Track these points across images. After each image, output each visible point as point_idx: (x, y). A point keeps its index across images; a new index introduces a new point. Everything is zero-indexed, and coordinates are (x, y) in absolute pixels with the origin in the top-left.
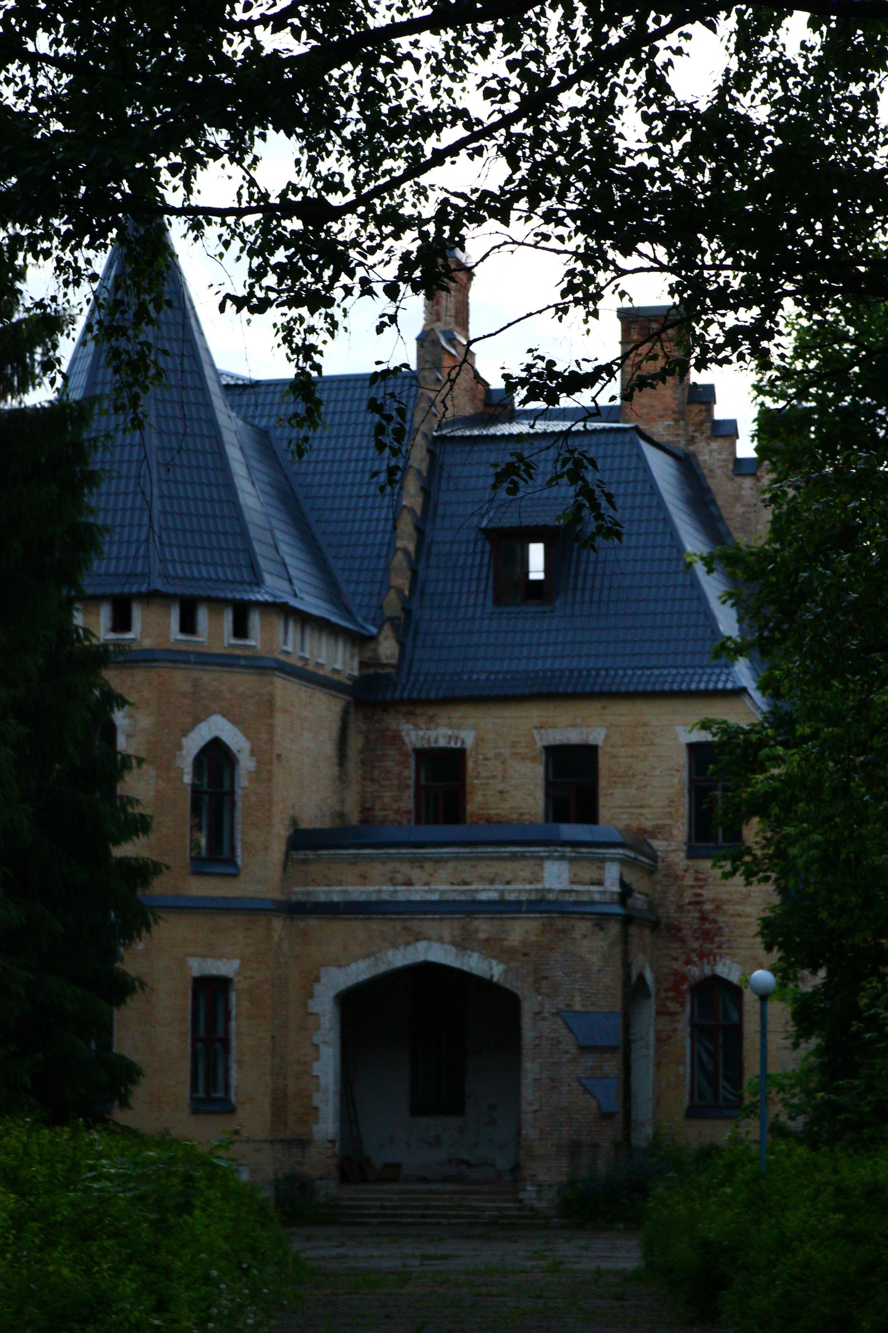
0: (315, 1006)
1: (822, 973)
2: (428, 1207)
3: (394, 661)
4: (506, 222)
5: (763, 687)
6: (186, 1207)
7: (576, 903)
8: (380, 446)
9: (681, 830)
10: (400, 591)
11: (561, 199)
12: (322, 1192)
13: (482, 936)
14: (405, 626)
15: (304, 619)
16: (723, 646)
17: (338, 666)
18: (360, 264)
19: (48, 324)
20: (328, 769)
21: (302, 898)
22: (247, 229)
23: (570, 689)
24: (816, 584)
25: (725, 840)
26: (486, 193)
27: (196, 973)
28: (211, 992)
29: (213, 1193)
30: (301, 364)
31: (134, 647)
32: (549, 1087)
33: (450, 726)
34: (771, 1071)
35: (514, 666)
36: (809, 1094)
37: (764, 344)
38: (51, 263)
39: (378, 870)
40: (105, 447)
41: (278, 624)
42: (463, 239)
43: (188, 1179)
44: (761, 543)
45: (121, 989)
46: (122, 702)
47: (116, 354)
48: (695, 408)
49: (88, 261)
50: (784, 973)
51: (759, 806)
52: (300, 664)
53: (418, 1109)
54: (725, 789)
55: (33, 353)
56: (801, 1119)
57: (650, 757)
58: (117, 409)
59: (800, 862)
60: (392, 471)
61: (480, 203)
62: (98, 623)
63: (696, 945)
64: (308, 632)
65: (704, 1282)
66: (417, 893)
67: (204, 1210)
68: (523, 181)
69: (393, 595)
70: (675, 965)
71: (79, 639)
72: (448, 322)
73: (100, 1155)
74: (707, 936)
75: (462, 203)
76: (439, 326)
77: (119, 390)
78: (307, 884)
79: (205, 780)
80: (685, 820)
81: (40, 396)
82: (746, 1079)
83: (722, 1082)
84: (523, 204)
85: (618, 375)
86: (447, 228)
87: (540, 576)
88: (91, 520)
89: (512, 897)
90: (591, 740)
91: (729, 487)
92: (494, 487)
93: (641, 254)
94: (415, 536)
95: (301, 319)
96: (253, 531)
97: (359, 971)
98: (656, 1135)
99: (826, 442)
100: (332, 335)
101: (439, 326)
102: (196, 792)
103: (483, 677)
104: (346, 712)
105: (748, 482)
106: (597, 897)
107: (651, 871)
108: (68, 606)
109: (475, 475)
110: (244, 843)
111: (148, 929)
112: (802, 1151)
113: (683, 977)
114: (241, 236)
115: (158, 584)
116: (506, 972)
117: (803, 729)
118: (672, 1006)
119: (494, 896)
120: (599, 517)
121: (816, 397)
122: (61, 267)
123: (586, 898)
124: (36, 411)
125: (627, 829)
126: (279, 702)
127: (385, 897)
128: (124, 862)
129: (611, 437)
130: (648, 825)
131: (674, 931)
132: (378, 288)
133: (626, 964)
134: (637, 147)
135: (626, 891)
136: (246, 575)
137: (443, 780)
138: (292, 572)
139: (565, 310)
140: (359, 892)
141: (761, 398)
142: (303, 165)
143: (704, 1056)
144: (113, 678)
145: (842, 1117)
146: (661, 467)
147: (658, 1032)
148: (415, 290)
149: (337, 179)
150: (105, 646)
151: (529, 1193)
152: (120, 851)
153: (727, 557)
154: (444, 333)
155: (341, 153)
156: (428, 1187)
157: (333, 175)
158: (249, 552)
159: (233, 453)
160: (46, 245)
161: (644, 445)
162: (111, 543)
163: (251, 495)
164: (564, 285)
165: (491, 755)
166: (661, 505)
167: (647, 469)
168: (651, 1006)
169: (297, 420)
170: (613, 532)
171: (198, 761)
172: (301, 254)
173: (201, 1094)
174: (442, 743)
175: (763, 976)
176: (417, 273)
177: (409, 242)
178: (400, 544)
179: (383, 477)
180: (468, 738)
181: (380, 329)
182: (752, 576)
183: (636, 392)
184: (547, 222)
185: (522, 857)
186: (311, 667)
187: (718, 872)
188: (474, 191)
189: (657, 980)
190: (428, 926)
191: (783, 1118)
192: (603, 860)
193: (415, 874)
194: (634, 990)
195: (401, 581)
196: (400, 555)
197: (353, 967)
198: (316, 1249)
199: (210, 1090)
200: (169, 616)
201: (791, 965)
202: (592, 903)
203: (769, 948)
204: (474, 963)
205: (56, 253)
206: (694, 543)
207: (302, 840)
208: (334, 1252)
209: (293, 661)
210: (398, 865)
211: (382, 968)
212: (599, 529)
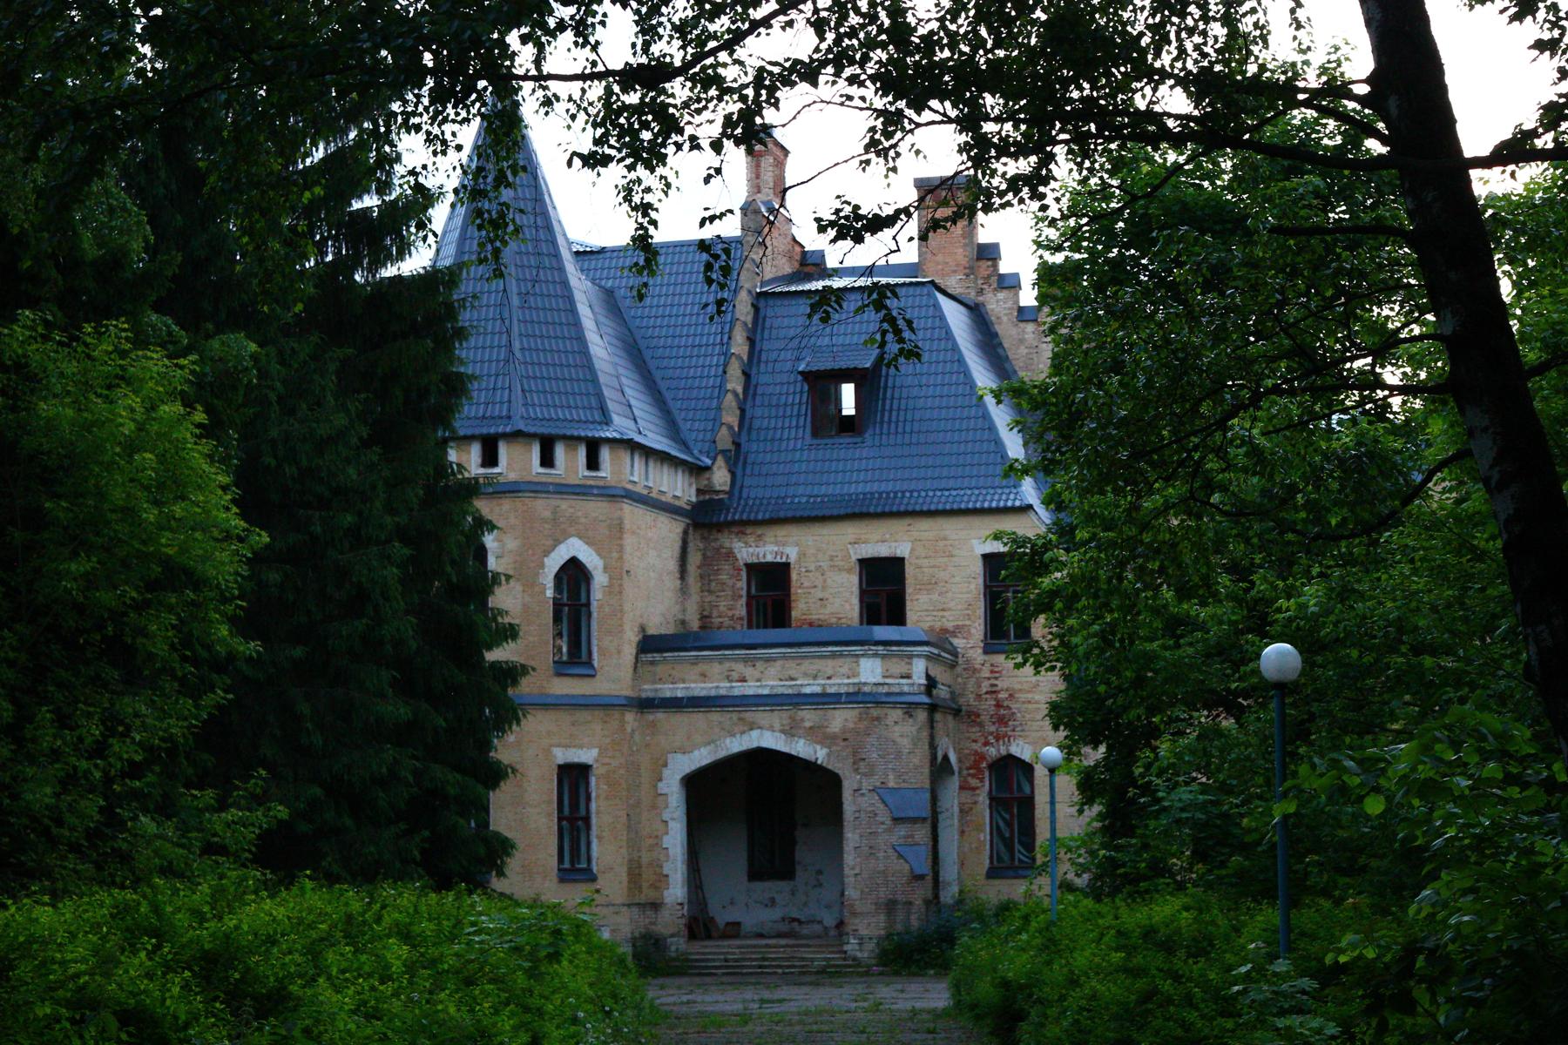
0: (662, 787)
1: (1102, 749)
2: (764, 959)
3: (727, 488)
4: (815, 84)
5: (1046, 502)
6: (555, 957)
7: (888, 694)
8: (709, 281)
9: (978, 629)
10: (730, 428)
11: (862, 67)
12: (673, 948)
13: (808, 724)
14: (736, 458)
15: (648, 453)
16: (1011, 467)
17: (678, 493)
18: (689, 123)
19: (424, 197)
20: (672, 582)
21: (651, 695)
22: (591, 104)
23: (879, 510)
24: (1090, 403)
25: (1016, 637)
26: (797, 62)
27: (561, 761)
28: (573, 778)
29: (577, 948)
30: (640, 220)
31: (501, 480)
32: (869, 856)
33: (776, 543)
34: (1059, 835)
35: (830, 490)
36: (1093, 853)
37: (1041, 189)
38: (422, 136)
39: (716, 669)
40: (473, 307)
41: (625, 456)
42: (777, 100)
43: (557, 933)
44: (1043, 376)
45: (495, 775)
46: (492, 527)
47: (479, 213)
48: (985, 264)
49: (454, 134)
50: (1070, 750)
51: (1044, 606)
52: (645, 492)
53: (755, 875)
54: (1016, 592)
55: (408, 227)
56: (1086, 876)
57: (949, 568)
58: (481, 261)
59: (1081, 650)
60: (720, 303)
61: (792, 70)
62: (469, 461)
63: (993, 729)
64: (651, 464)
65: (1005, 1015)
66: (750, 689)
67: (571, 962)
68: (829, 50)
69: (724, 430)
70: (975, 746)
71: (453, 473)
72: (767, 194)
73: (480, 914)
74: (1002, 721)
75: (776, 70)
76: (760, 197)
77: (481, 245)
78: (654, 682)
79: (565, 595)
80: (982, 621)
81: (418, 260)
82: (1038, 843)
83: (1017, 846)
84: (830, 69)
85: (915, 216)
86: (764, 92)
87: (852, 412)
88: (462, 370)
89: (832, 690)
90: (899, 554)
91: (1014, 331)
92: (810, 316)
93: (931, 109)
94: (742, 379)
95: (639, 181)
96: (602, 379)
97: (702, 757)
98: (961, 892)
99: (1099, 288)
100: (666, 194)
101: (760, 197)
102: (558, 606)
103: (804, 500)
104: (685, 533)
105: (1030, 327)
106: (906, 689)
107: (953, 666)
108: (444, 443)
109: (790, 319)
110: (599, 648)
111: (518, 723)
112: (1088, 903)
113: (982, 757)
114: (585, 109)
115: (522, 426)
116: (828, 755)
117: (1081, 535)
118: (974, 782)
119: (818, 689)
120: (901, 340)
121: (1087, 249)
122: (430, 139)
123: (896, 690)
124: (415, 280)
125: (932, 629)
126: (627, 525)
127: (723, 692)
128: (494, 664)
129: (911, 290)
130: (950, 625)
131: (972, 717)
132: (705, 143)
133: (933, 747)
134: (926, 16)
135: (931, 683)
136: (597, 416)
137: (771, 591)
138: (636, 412)
139: (868, 162)
140: (700, 689)
141: (1041, 252)
142: (639, 47)
143: (1002, 825)
144: (484, 506)
145: (1122, 871)
146: (955, 317)
147: (961, 804)
148: (737, 144)
149: (668, 59)
150: (476, 479)
151: (852, 946)
152: (492, 656)
153: (1014, 391)
154: (764, 203)
155: (671, 37)
156: (764, 942)
157: (664, 56)
158: (600, 396)
159: (584, 310)
160: (416, 120)
161: (940, 297)
162: (480, 390)
163: (601, 347)
164: (867, 140)
165: (812, 568)
166: (955, 348)
167: (942, 318)
168: (955, 782)
169: (638, 269)
170: (914, 354)
171: (558, 577)
172: (636, 125)
173: (567, 865)
174: (769, 558)
175: (1052, 752)
176: (739, 130)
177: (733, 106)
178: (729, 386)
179: (712, 309)
180: (792, 554)
181: (707, 180)
182: (1036, 406)
183: (931, 235)
184: (851, 84)
185: (841, 655)
186: (653, 495)
187: (1011, 664)
188: (787, 60)
189: (960, 761)
190: (761, 716)
191: (1070, 876)
192: (911, 657)
193: (748, 671)
194: (940, 769)
195: (731, 418)
196: (730, 396)
197: (696, 753)
198: (668, 995)
199: (574, 862)
200: (530, 451)
201: (1075, 743)
202: (901, 694)
203: (1056, 728)
204: (801, 748)
205: (425, 127)
206: (983, 378)
207: (650, 645)
208: (685, 998)
209: (639, 489)
210: (734, 665)
211: (722, 754)
212: (901, 351)
